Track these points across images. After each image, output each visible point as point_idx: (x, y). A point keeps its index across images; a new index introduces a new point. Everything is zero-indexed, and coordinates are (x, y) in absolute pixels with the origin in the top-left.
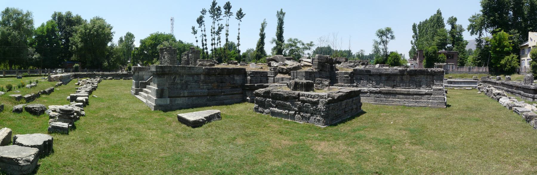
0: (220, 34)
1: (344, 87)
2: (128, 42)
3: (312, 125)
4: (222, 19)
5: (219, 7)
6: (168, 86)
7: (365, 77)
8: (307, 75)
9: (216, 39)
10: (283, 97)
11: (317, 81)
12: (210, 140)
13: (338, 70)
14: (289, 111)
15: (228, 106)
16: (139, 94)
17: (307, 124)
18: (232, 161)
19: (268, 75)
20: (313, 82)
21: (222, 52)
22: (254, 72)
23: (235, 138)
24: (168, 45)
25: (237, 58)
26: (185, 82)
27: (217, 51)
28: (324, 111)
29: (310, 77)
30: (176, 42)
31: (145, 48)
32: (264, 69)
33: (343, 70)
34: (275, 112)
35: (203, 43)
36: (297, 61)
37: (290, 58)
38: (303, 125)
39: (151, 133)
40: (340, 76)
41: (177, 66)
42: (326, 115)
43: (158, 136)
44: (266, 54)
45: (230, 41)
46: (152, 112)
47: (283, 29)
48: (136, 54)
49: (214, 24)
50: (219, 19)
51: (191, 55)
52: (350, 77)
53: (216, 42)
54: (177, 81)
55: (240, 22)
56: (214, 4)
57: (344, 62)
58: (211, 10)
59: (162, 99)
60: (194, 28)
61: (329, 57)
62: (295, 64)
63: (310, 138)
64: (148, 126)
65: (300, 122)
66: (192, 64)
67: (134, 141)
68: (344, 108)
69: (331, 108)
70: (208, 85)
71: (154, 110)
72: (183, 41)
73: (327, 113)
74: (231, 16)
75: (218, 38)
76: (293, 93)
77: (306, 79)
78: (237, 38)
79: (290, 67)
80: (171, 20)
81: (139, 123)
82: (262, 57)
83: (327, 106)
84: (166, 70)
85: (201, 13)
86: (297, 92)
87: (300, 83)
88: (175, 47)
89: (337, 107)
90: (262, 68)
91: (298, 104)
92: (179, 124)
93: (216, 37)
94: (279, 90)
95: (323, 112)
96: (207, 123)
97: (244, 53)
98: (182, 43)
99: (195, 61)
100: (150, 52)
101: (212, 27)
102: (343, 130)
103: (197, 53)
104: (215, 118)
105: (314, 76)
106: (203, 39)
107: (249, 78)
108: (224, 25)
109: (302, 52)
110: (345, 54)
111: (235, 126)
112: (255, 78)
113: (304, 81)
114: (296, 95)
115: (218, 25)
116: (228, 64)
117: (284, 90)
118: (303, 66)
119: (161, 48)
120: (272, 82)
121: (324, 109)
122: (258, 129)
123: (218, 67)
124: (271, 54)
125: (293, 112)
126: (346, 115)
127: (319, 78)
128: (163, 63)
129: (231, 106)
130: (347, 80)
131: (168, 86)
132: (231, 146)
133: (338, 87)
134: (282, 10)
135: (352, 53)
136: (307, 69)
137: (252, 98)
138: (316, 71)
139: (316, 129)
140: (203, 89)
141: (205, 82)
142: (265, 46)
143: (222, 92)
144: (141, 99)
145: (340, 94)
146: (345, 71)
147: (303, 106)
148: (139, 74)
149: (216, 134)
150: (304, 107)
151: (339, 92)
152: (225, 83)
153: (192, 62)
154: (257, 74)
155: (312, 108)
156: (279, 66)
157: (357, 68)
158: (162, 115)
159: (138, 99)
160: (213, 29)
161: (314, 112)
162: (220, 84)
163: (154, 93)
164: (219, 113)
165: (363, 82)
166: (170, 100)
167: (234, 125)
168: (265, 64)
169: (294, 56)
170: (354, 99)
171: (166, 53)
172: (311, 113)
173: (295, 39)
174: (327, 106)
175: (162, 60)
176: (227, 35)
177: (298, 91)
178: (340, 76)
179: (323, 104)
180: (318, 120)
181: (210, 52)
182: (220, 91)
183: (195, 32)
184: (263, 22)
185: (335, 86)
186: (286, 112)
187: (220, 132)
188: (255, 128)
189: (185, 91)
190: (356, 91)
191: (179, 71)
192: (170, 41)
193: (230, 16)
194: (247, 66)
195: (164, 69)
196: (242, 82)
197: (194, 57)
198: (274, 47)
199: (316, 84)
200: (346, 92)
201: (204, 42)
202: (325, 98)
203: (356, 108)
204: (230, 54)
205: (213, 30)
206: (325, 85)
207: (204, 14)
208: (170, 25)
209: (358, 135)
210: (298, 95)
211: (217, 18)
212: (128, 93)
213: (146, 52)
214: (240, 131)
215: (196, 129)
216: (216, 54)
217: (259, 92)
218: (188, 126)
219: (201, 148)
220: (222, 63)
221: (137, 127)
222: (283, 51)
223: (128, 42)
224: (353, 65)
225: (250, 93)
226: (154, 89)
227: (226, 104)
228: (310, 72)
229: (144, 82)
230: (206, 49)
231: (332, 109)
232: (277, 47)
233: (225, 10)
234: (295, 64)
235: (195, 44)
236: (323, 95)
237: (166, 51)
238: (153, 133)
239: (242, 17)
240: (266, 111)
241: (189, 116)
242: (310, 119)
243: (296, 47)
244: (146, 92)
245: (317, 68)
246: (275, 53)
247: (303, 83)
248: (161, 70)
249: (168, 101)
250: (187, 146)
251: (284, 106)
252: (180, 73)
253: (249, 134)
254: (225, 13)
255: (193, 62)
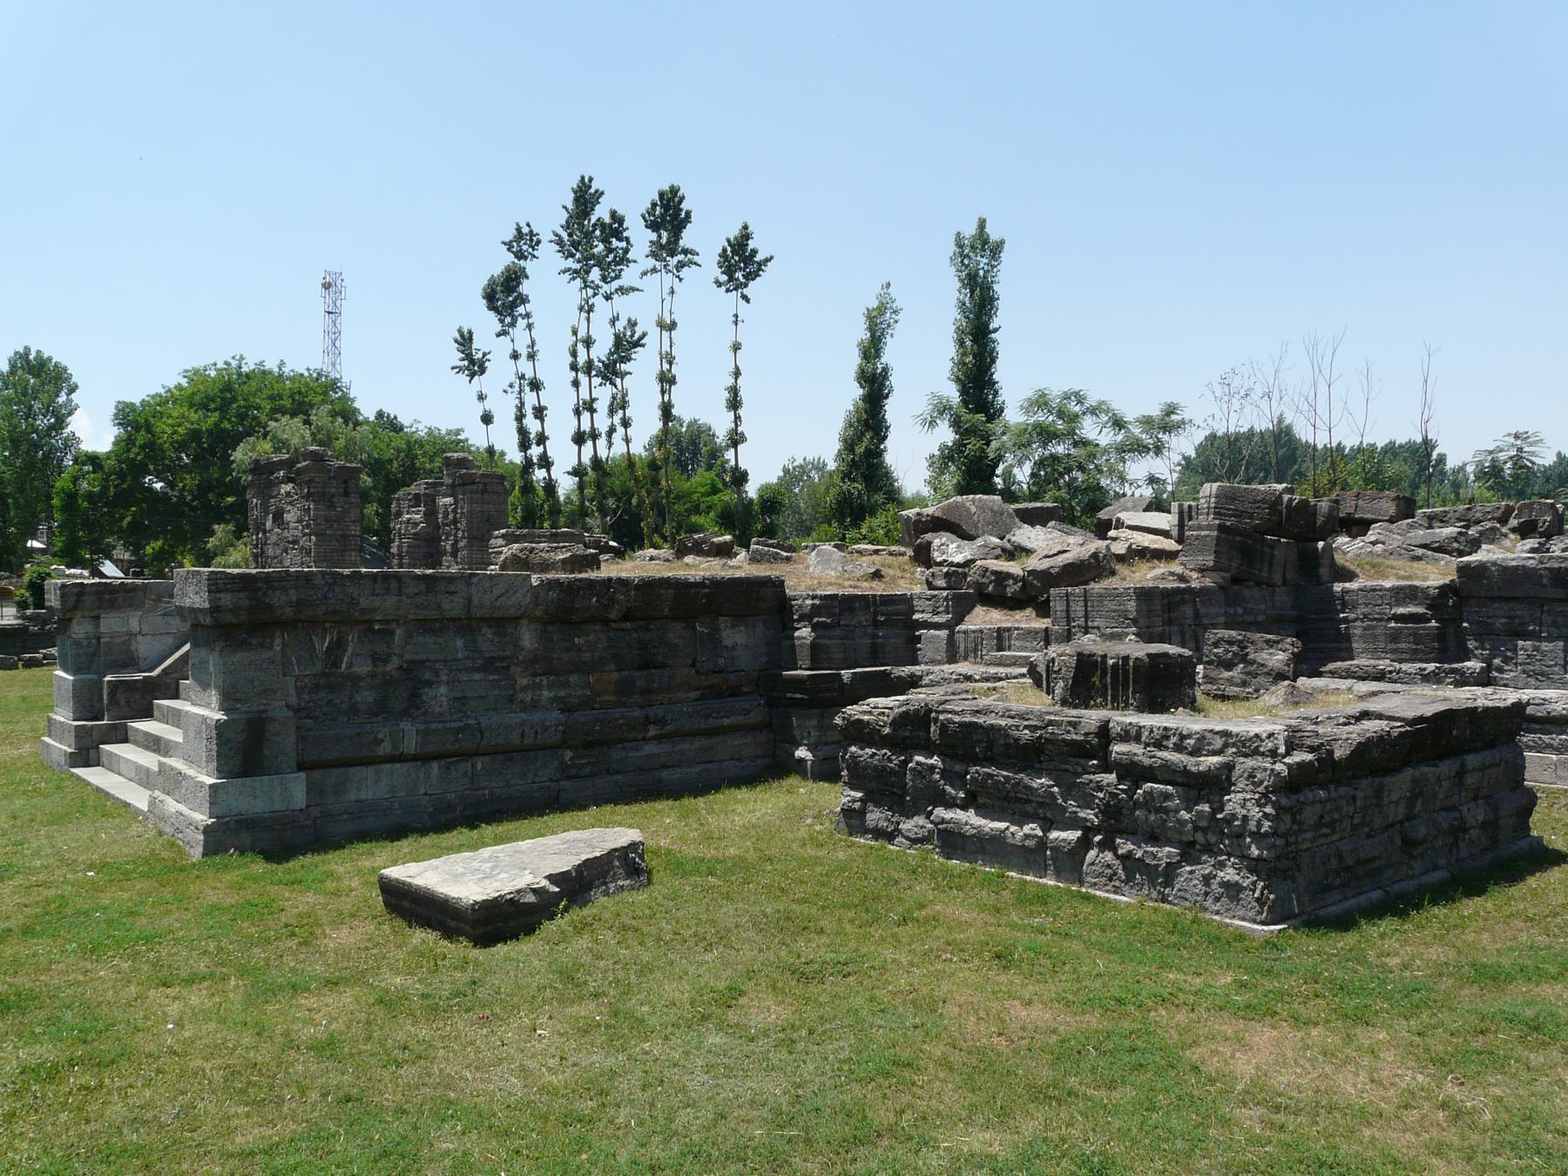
0: (623, 375)
1: (1398, 687)
2: (30, 414)
3: (1190, 916)
4: (634, 289)
5: (613, 214)
6: (293, 700)
7: (1547, 619)
8: (1150, 612)
9: (602, 406)
10: (1007, 746)
11: (1216, 645)
12: (586, 1009)
13: (1349, 576)
14: (1046, 830)
15: (687, 802)
16: (104, 759)
17: (1155, 910)
18: (722, 1129)
19: (916, 616)
20: (1187, 652)
21: (636, 479)
22: (835, 596)
23: (735, 992)
24: (305, 444)
25: (727, 519)
26: (400, 668)
27: (606, 474)
28: (1266, 835)
29: (1169, 622)
30: (357, 424)
31: (146, 456)
32: (894, 578)
33: (1385, 577)
34: (962, 836)
35: (523, 432)
36: (1084, 527)
37: (1042, 508)
38: (1131, 916)
39: (170, 1005)
40: (1361, 610)
41: (347, 571)
42: (1278, 858)
43: (222, 1021)
44: (899, 490)
45: (687, 418)
46: (194, 865)
47: (993, 336)
48: (89, 497)
49: (588, 319)
50: (616, 284)
51: (449, 500)
52: (1433, 617)
53: (602, 422)
54: (350, 665)
55: (742, 302)
56: (585, 198)
57: (1392, 521)
58: (570, 235)
59: (260, 783)
60: (471, 339)
61: (1286, 497)
62: (1077, 546)
63: (1180, 995)
64: (157, 965)
65: (1115, 892)
66: (454, 554)
67: (53, 1074)
68: (1401, 822)
69: (1310, 815)
70: (566, 685)
71: (205, 855)
72: (404, 420)
73: (1288, 844)
74: (686, 268)
75: (614, 398)
76: (1069, 722)
77: (1146, 636)
78: (728, 400)
79: (1044, 565)
80: (327, 286)
81: (93, 951)
82: (873, 511)
83: (1284, 801)
84: (280, 600)
85: (505, 248)
86: (1092, 717)
87: (1111, 662)
88: (348, 452)
89: (1351, 810)
90: (877, 575)
91: (1100, 788)
92: (389, 928)
93: (604, 394)
94: (984, 702)
95: (1258, 836)
96: (566, 910)
97: (765, 488)
98: (394, 426)
99: (479, 540)
100: (190, 481)
101: (575, 333)
102: (1397, 960)
103: (484, 491)
104: (614, 880)
105: (1197, 616)
106: (522, 404)
107: (804, 633)
108: (647, 325)
109: (1111, 471)
110: (1392, 469)
111: (730, 922)
112: (838, 632)
113: (1135, 649)
114: (1086, 734)
115: (613, 321)
116: (681, 552)
117: (1016, 706)
118: (1121, 559)
119: (257, 461)
120: (942, 655)
121: (1267, 824)
122: (869, 936)
123: (624, 575)
124: (926, 491)
125: (1073, 835)
126: (1418, 866)
127: (1228, 626)
128: (270, 552)
129: (701, 801)
130: (1417, 638)
131: (293, 700)
132: (715, 1039)
133: (1349, 682)
134: (982, 224)
135: (1442, 459)
136: (1149, 575)
137: (825, 751)
138: (1208, 582)
139: (1214, 940)
140: (535, 705)
141: (542, 664)
142: (888, 443)
143: (647, 722)
144: (112, 792)
145: (1373, 727)
146: (1399, 578)
147: (1131, 798)
148: (97, 626)
149: (621, 975)
150: (1137, 805)
151: (1365, 715)
152: (662, 666)
153: (456, 541)
154: (852, 610)
155: (1189, 810)
156: (977, 563)
157: (1485, 554)
158: (256, 880)
159: (98, 790)
160: (580, 347)
161: (1200, 837)
162: (636, 674)
163: (204, 747)
164: (633, 846)
165: (1536, 649)
166: (311, 788)
167: (727, 913)
168: (893, 548)
169: (1063, 493)
170: (1472, 760)
171: (288, 494)
172: (1181, 842)
173: (1066, 397)
174: (1284, 801)
175: (265, 532)
176: (667, 380)
177: (1097, 706)
178: (1365, 610)
179: (1260, 789)
180: (1225, 885)
181: (566, 485)
182: (637, 713)
183: (472, 362)
184: (874, 304)
185: (1333, 674)
186: (1027, 836)
187: (646, 957)
188: (848, 928)
189: (406, 725)
190: (1487, 710)
191: (364, 602)
192: (320, 416)
193: (685, 272)
194: (788, 568)
195: (265, 594)
196: (764, 659)
197: (471, 516)
198: (943, 448)
199: (1209, 663)
200: (1410, 714)
201: (533, 425)
202: (1273, 753)
203: (1490, 826)
204: (690, 493)
205: (581, 349)
206: (1268, 674)
207: (526, 258)
208: (319, 321)
209: (1529, 1013)
210: (1097, 735)
211: (604, 279)
212: (20, 757)
213: (158, 486)
214: (761, 950)
215: (501, 949)
216: (605, 497)
217: (866, 718)
218: (449, 934)
219: (532, 1064)
220: (641, 547)
221: (81, 978)
222: (999, 471)
223: (27, 416)
224: (1456, 540)
225: (814, 722)
226: (204, 719)
227: (675, 792)
228: (1166, 593)
229: (139, 676)
230: (541, 467)
231: (1319, 824)
232: (959, 446)
233: (654, 236)
234: (1077, 546)
235: (477, 438)
236: (1257, 736)
237: (290, 480)
238: (194, 1000)
239: (751, 276)
240: (907, 825)
241: (457, 877)
242: (1180, 882)
243: (1075, 444)
244: (155, 744)
245: (1212, 569)
246: (950, 479)
247: (1126, 658)
248: (244, 599)
249: (295, 791)
250: (447, 1059)
251: (1018, 800)
252: (366, 617)
253: (816, 966)
254: (654, 255)
255: (462, 544)
